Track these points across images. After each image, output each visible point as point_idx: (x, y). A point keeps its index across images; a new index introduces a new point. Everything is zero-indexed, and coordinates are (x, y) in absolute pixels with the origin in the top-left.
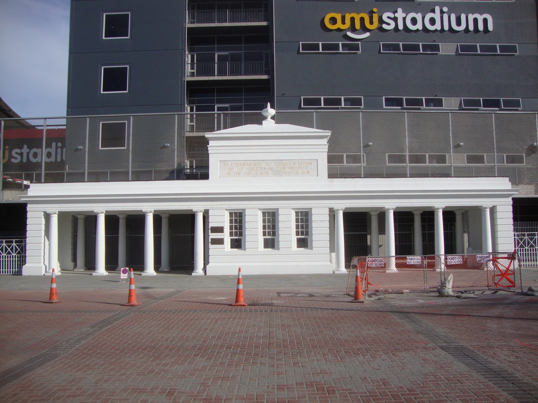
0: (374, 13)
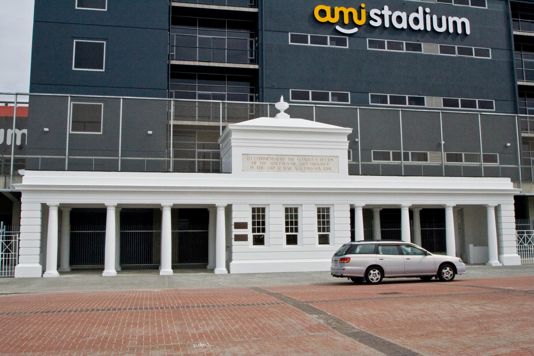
0: (362, 8)
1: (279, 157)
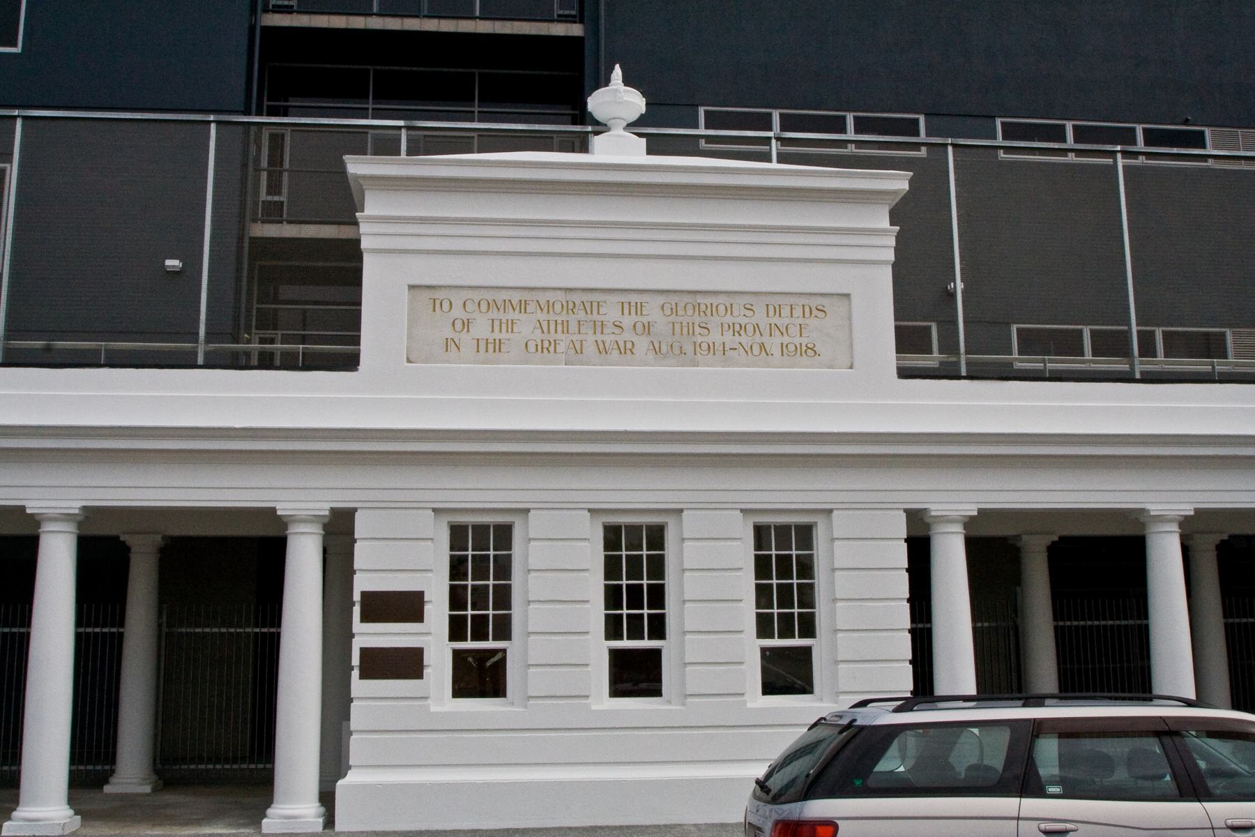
1: (577, 298)
